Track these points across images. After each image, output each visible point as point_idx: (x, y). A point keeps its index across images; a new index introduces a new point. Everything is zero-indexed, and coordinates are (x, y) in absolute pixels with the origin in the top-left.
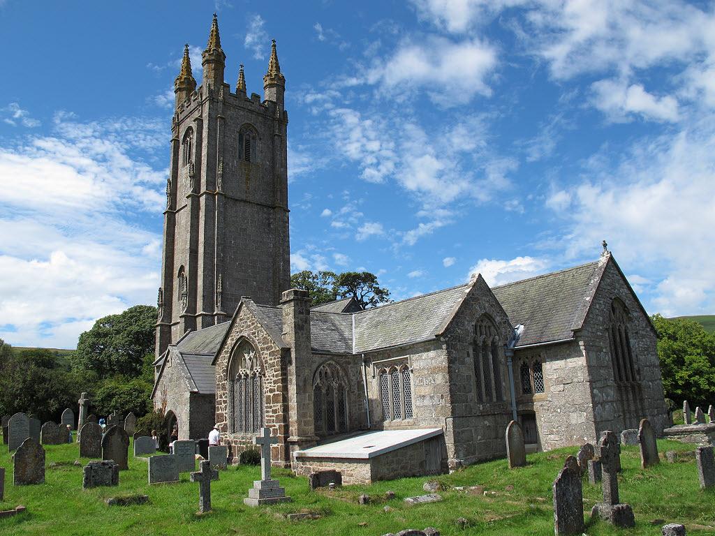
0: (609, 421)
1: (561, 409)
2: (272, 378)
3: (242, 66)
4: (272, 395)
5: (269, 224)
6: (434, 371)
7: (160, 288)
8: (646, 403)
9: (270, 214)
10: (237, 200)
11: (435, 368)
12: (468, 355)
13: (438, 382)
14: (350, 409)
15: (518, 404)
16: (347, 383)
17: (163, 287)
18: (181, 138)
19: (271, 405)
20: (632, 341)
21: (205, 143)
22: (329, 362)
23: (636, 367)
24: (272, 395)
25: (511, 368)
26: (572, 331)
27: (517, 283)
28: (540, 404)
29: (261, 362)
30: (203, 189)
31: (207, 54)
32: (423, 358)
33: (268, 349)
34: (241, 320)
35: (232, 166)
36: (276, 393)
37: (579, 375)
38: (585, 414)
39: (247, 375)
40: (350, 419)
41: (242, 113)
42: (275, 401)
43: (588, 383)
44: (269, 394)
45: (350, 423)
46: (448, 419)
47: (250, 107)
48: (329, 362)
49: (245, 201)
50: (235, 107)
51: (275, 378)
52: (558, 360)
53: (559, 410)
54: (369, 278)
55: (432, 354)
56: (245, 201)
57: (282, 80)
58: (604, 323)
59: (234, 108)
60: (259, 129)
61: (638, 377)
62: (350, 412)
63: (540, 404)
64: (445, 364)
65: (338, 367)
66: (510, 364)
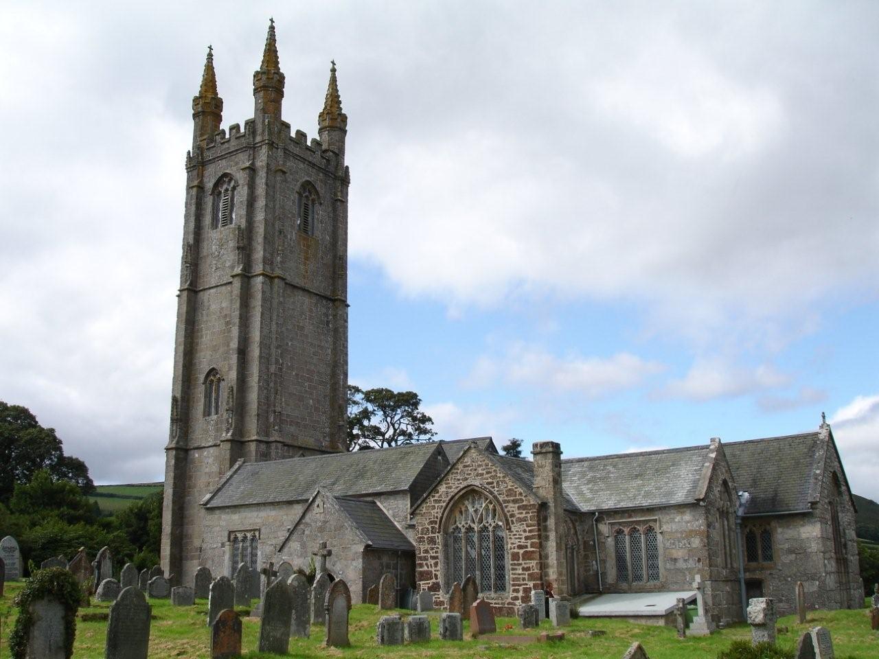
2: (522, 533)
4: (521, 551)
5: (328, 323)
6: (690, 534)
11: (691, 531)
13: (694, 546)
15: (746, 570)
18: (210, 185)
19: (521, 562)
21: (261, 203)
24: (521, 551)
26: (809, 502)
28: (769, 572)
29: (505, 516)
30: (258, 268)
31: (264, 77)
32: (676, 520)
33: (515, 501)
34: (465, 466)
36: (529, 549)
38: (817, 583)
39: (470, 529)
40: (579, 581)
41: (302, 166)
42: (528, 556)
43: (822, 554)
44: (516, 550)
45: (579, 586)
47: (310, 159)
49: (304, 290)
50: (296, 156)
51: (527, 534)
52: (173, 516)
54: (409, 400)
55: (687, 517)
56: (304, 290)
58: (828, 496)
60: (319, 189)
61: (844, 551)
62: (578, 574)
63: (769, 572)
66: (739, 531)
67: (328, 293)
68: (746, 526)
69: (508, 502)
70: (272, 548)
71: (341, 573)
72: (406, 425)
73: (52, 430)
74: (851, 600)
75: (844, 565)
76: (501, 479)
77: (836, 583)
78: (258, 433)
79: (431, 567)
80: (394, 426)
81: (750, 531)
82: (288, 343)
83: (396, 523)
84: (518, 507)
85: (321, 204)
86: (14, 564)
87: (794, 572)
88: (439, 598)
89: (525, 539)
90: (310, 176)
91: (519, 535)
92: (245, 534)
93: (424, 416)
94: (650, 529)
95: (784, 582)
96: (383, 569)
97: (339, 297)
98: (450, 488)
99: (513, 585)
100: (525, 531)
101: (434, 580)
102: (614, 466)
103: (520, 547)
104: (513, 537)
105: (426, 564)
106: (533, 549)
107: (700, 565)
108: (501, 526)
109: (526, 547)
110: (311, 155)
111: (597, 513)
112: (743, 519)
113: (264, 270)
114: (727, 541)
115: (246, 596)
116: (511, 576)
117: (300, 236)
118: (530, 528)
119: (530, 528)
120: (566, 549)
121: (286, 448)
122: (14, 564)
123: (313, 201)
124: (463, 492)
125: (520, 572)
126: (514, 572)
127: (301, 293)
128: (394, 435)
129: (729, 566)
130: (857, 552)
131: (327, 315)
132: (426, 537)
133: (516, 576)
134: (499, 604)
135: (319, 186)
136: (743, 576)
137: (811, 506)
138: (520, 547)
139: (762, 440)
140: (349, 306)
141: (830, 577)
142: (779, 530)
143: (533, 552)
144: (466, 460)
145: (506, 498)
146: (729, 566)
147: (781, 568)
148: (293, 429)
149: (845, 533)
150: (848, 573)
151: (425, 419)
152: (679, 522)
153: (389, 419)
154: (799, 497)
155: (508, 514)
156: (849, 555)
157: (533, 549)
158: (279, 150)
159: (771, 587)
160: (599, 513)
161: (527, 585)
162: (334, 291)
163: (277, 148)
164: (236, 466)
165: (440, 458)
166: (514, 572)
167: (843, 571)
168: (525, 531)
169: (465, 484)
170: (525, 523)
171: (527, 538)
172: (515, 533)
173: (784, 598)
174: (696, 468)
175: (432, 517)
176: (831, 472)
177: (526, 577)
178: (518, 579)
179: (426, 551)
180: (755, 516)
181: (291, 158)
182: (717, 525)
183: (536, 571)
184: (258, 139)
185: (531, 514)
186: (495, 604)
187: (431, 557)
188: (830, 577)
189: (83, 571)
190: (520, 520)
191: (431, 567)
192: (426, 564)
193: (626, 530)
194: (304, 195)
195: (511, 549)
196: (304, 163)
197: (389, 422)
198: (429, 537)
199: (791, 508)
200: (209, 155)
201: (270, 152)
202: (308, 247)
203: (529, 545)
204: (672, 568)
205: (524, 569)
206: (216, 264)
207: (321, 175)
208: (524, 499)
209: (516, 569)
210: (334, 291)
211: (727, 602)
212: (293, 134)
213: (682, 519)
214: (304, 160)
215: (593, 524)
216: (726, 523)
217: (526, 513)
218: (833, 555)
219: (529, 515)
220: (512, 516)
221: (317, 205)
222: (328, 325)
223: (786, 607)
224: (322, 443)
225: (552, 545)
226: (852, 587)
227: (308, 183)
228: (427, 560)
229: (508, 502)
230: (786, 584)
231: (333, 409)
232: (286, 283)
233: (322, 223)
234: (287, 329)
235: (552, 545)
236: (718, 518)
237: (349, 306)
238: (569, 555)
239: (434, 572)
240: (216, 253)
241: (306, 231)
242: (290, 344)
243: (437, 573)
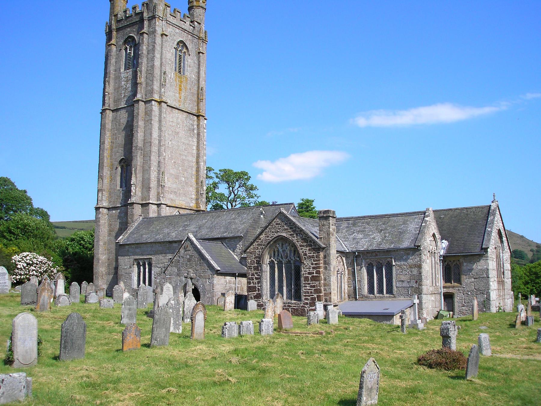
4: (310, 276)
24: (310, 276)
36: (315, 275)
41: (177, 31)
44: (307, 275)
51: (314, 266)
54: (242, 176)
61: (502, 276)
62: (344, 289)
67: (194, 111)
68: (445, 261)
69: (303, 246)
70: (160, 269)
71: (201, 286)
72: (242, 192)
73: (25, 192)
74: (505, 305)
75: (502, 285)
76: (299, 232)
77: (497, 295)
79: (256, 284)
80: (234, 193)
81: (448, 264)
83: (235, 256)
84: (309, 249)
86: (5, 283)
88: (260, 302)
90: (183, 38)
91: (309, 266)
92: (144, 261)
93: (252, 186)
96: (227, 284)
97: (201, 114)
98: (268, 237)
99: (305, 296)
100: (312, 264)
101: (257, 292)
102: (368, 224)
103: (309, 273)
105: (253, 282)
108: (298, 261)
109: (313, 273)
110: (184, 25)
112: (444, 257)
114: (434, 270)
115: (144, 304)
116: (304, 290)
117: (176, 75)
118: (316, 262)
119: (316, 262)
120: (337, 274)
121: (168, 208)
122: (5, 283)
124: (276, 239)
126: (306, 288)
128: (234, 199)
129: (434, 285)
130: (510, 277)
133: (307, 291)
134: (296, 307)
138: (309, 273)
139: (457, 209)
141: (493, 292)
142: (465, 264)
146: (434, 285)
148: (172, 196)
150: (504, 289)
151: (252, 188)
153: (231, 188)
156: (505, 279)
158: (163, 21)
161: (313, 296)
162: (198, 109)
165: (262, 216)
166: (306, 288)
167: (501, 289)
168: (312, 264)
169: (276, 235)
170: (312, 259)
171: (314, 268)
172: (306, 265)
174: (417, 226)
175: (257, 254)
176: (497, 229)
177: (313, 291)
178: (308, 293)
179: (253, 275)
182: (428, 261)
185: (316, 254)
186: (294, 306)
187: (256, 278)
188: (493, 292)
189: (46, 291)
190: (310, 257)
191: (256, 284)
192: (253, 282)
194: (179, 49)
195: (304, 274)
197: (231, 190)
198: (254, 266)
199: (473, 251)
202: (181, 82)
203: (315, 272)
205: (311, 287)
206: (124, 93)
207: (190, 36)
208: (313, 244)
209: (306, 287)
210: (198, 109)
211: (432, 306)
215: (354, 259)
216: (433, 259)
217: (313, 253)
218: (496, 279)
220: (305, 255)
221: (186, 57)
222: (193, 131)
224: (190, 204)
226: (506, 298)
227: (181, 42)
229: (303, 246)
231: (197, 184)
232: (167, 105)
233: (190, 67)
234: (168, 134)
236: (429, 256)
238: (339, 278)
239: (257, 287)
240: (124, 86)
241: (180, 72)
242: (170, 144)
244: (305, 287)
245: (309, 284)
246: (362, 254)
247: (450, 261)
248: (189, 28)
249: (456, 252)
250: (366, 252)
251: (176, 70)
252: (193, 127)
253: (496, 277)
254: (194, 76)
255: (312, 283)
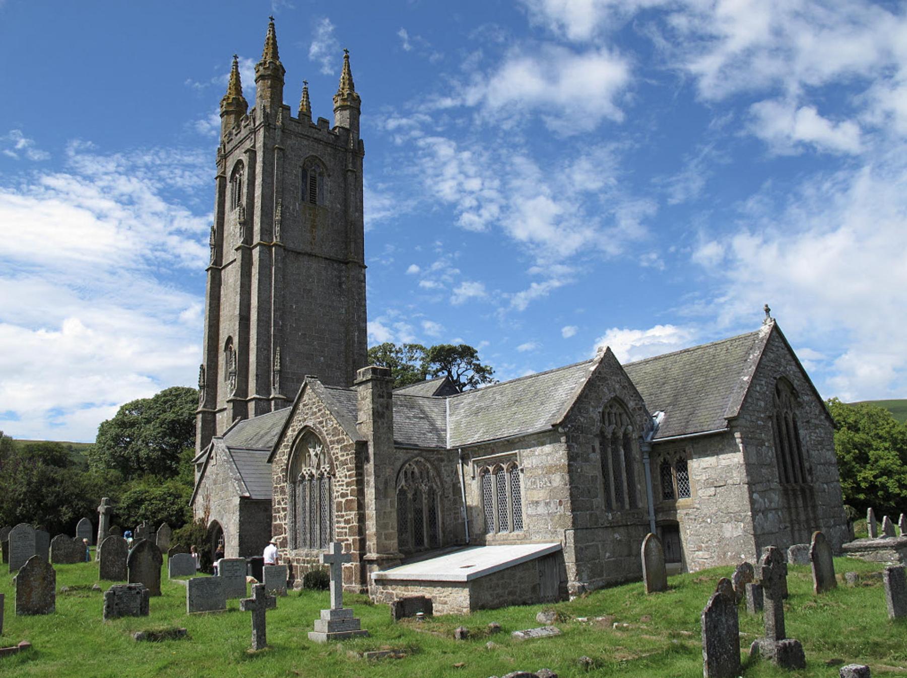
0: (773, 533)
1: (711, 518)
2: (344, 479)
3: (306, 83)
4: (343, 500)
5: (340, 284)
6: (550, 470)
7: (202, 365)
8: (820, 512)
9: (342, 271)
10: (299, 253)
11: (551, 467)
12: (594, 450)
14: (443, 518)
16: (439, 484)
17: (205, 364)
18: (229, 174)
19: (343, 513)
20: (802, 432)
22: (416, 459)
23: (807, 465)
25: (648, 467)
27: (656, 359)
28: (685, 512)
30: (257, 239)
31: (261, 68)
32: (537, 453)
35: (294, 210)
36: (350, 498)
37: (734, 475)
39: (312, 476)
41: (305, 142)
42: (348, 508)
46: (568, 531)
47: (316, 136)
48: (416, 459)
49: (310, 255)
50: (297, 135)
53: (709, 520)
54: (467, 352)
56: (310, 255)
57: (358, 100)
59: (295, 136)
60: (327, 163)
62: (443, 523)
63: (685, 512)
64: (564, 461)
65: (428, 465)
67: (341, 257)
78: (257, 393)
81: (665, 459)
82: (292, 306)
85: (329, 176)
87: (714, 511)
89: (347, 486)
94: (515, 467)
95: (703, 524)
104: (337, 484)
106: (352, 498)
107: (561, 510)
109: (347, 495)
110: (317, 133)
111: (460, 450)
113: (261, 240)
123: (321, 174)
125: (342, 525)
127: (306, 257)
131: (339, 277)
132: (279, 486)
135: (326, 159)
136: (654, 518)
137: (729, 423)
140: (366, 267)
143: (351, 500)
144: (304, 399)
145: (332, 439)
147: (698, 506)
149: (809, 456)
152: (539, 455)
154: (717, 413)
155: (334, 457)
157: (352, 498)
159: (688, 531)
160: (462, 449)
163: (275, 129)
164: (237, 421)
173: (703, 545)
180: (686, 438)
181: (293, 136)
183: (355, 524)
184: (257, 124)
193: (491, 468)
196: (308, 140)
199: (705, 428)
200: (229, 147)
201: (267, 133)
204: (534, 513)
207: (329, 149)
212: (315, 121)
213: (542, 452)
214: (308, 137)
219: (348, 457)
223: (707, 557)
225: (370, 493)
228: (279, 512)
230: (706, 527)
235: (370, 493)
237: (366, 267)
241: (313, 201)
243: (286, 527)
244: (338, 522)
245: (342, 516)
246: (472, 451)
247: (668, 454)
248: (328, 138)
249: (673, 433)
250: (476, 446)
251: (303, 199)
252: (340, 280)
253: (778, 480)
254: (338, 206)
255: (347, 515)
